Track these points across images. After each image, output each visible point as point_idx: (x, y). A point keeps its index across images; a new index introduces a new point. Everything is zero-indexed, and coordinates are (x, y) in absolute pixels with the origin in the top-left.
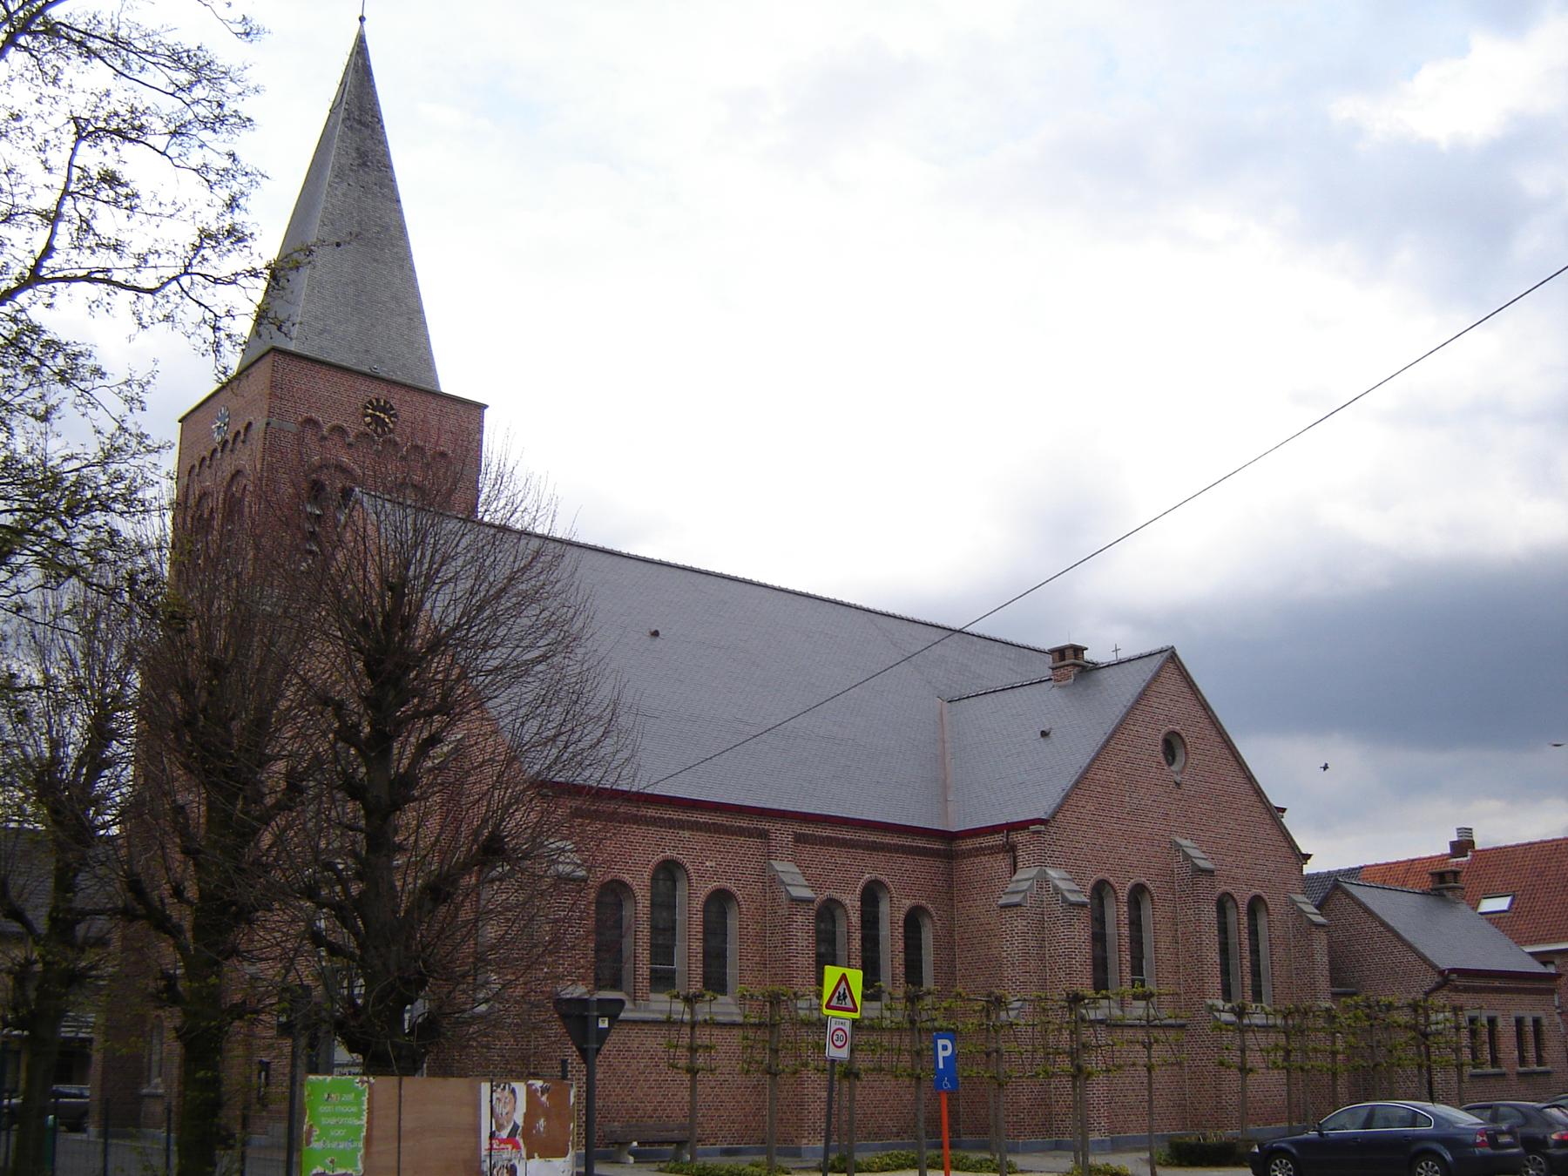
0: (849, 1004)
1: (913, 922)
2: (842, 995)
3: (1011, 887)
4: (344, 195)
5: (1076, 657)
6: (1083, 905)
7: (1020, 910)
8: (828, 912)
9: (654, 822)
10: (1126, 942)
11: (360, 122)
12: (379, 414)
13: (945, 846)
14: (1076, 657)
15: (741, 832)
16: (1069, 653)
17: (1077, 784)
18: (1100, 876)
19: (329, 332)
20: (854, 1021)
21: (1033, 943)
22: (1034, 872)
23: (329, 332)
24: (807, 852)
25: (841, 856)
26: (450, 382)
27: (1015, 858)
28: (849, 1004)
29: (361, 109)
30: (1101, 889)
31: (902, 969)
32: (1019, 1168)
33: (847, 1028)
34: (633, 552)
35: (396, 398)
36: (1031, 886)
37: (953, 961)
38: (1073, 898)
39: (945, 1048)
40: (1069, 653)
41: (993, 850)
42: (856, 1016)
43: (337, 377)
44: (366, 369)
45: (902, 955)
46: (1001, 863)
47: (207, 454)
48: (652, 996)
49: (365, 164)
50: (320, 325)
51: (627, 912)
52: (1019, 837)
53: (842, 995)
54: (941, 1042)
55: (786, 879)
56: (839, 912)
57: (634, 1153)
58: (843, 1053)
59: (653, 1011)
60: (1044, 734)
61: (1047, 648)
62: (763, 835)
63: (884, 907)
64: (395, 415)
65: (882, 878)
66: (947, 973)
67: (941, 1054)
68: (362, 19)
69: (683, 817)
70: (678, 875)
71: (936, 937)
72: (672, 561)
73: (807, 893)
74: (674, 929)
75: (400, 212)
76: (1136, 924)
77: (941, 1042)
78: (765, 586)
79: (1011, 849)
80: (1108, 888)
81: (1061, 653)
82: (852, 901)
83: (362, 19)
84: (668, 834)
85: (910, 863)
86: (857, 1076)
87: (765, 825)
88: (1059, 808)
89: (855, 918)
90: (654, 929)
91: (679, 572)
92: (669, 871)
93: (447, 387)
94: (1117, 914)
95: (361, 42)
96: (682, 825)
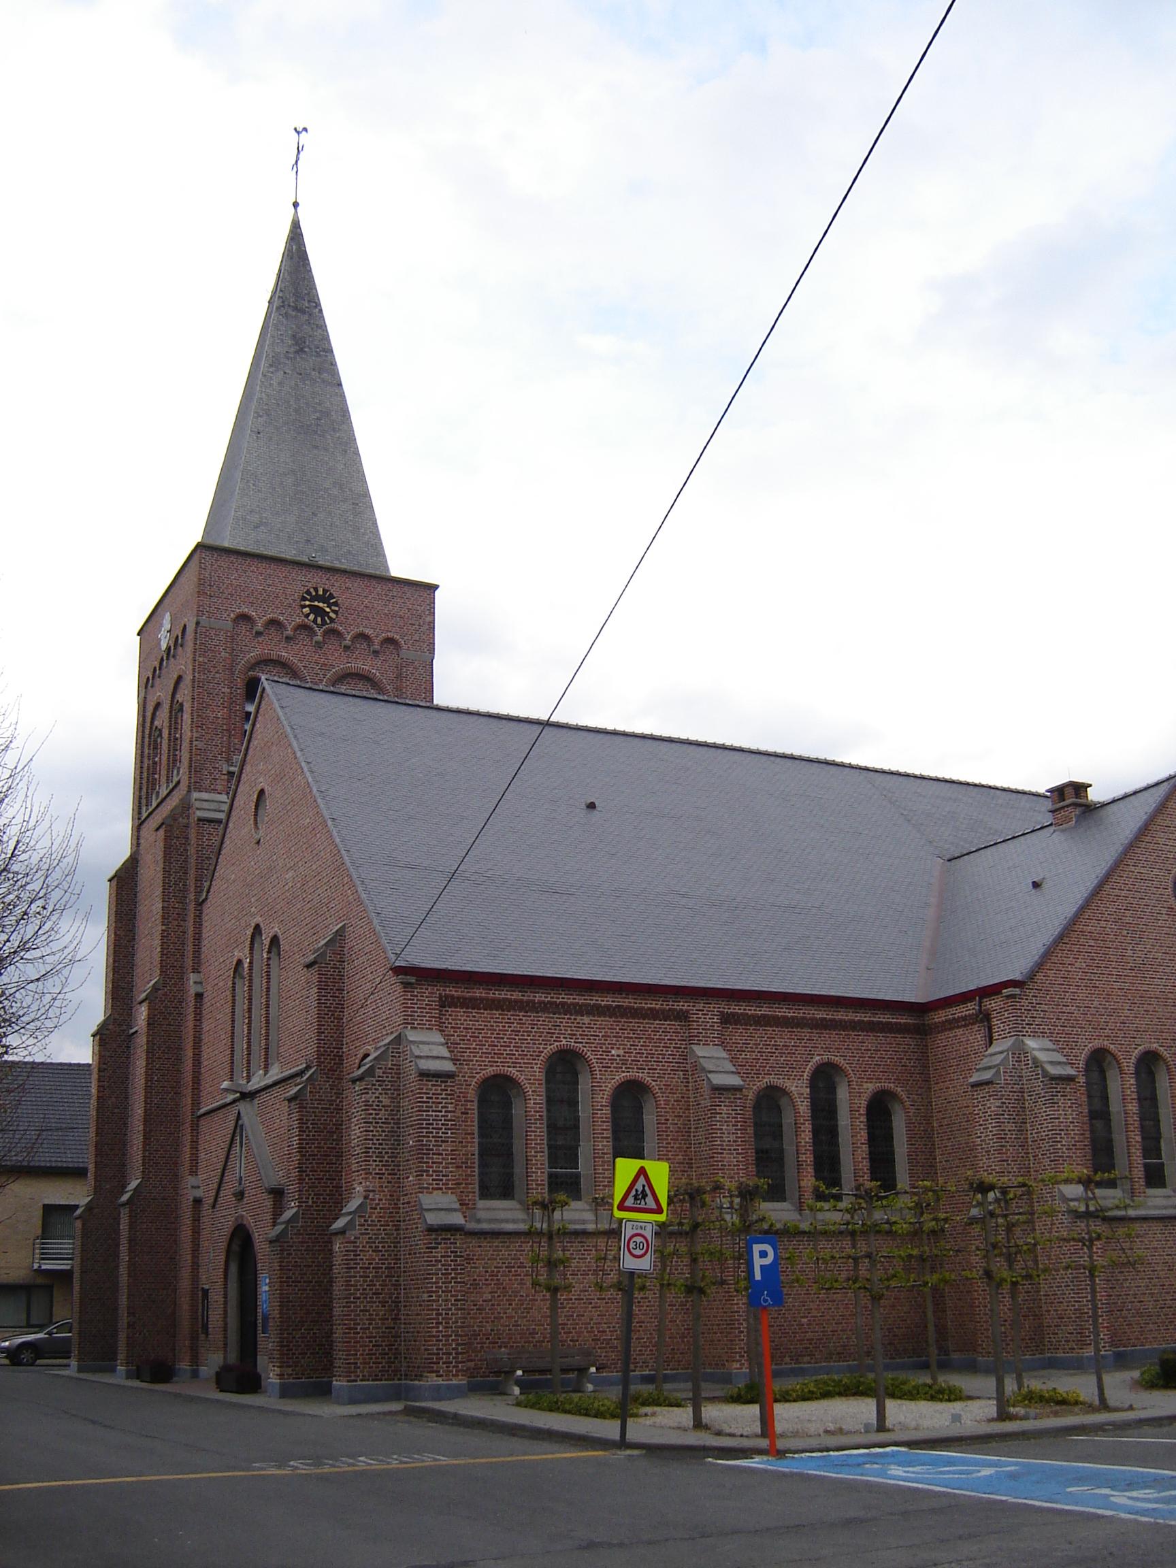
0: (650, 1203)
1: (879, 1111)
2: (641, 1192)
3: (986, 1062)
4: (280, 383)
5: (1077, 795)
6: (1070, 1079)
7: (992, 1088)
8: (770, 1101)
9: (545, 1007)
10: (1134, 1120)
11: (296, 309)
12: (320, 605)
13: (915, 1021)
14: (1077, 795)
15: (654, 1014)
16: (1069, 791)
17: (1061, 938)
18: (1097, 1043)
19: (266, 524)
20: (662, 1225)
21: (1009, 1126)
22: (1009, 1043)
23: (266, 524)
24: (738, 1035)
25: (782, 1037)
26: (400, 566)
27: (990, 1029)
28: (650, 1203)
29: (297, 296)
30: (1099, 1061)
31: (866, 1163)
32: (965, 1393)
33: (648, 1233)
34: (846, 761)
35: (336, 586)
36: (1006, 1058)
37: (932, 1152)
38: (1053, 1071)
39: (763, 1254)
40: (1069, 791)
41: (967, 1022)
42: (662, 1218)
43: (271, 569)
44: (305, 559)
45: (865, 1148)
46: (976, 1035)
47: (157, 664)
48: (481, 1204)
49: (302, 350)
50: (255, 518)
51: (517, 1110)
52: (992, 1004)
53: (641, 1192)
54: (756, 1248)
55: (709, 1066)
56: (784, 1101)
57: (518, 1382)
58: (644, 1264)
59: (479, 1221)
60: (1036, 885)
61: (1042, 790)
62: (683, 1016)
63: (842, 1094)
64: (336, 604)
65: (837, 1060)
66: (925, 1164)
67: (758, 1262)
68: (296, 205)
69: (580, 1000)
70: (579, 1067)
71: (909, 1124)
72: (710, 740)
73: (735, 1081)
74: (576, 1127)
75: (343, 395)
76: (1148, 1100)
77: (756, 1248)
78: (741, 750)
79: (985, 1018)
80: (1109, 1058)
81: (1059, 792)
82: (799, 1088)
83: (296, 205)
84: (563, 1020)
85: (871, 1041)
86: (701, 1291)
87: (682, 1005)
88: (1040, 966)
89: (804, 1107)
90: (552, 1128)
91: (592, 735)
92: (565, 1067)
93: (396, 571)
94: (1122, 1089)
95: (296, 227)
96: (580, 1010)
